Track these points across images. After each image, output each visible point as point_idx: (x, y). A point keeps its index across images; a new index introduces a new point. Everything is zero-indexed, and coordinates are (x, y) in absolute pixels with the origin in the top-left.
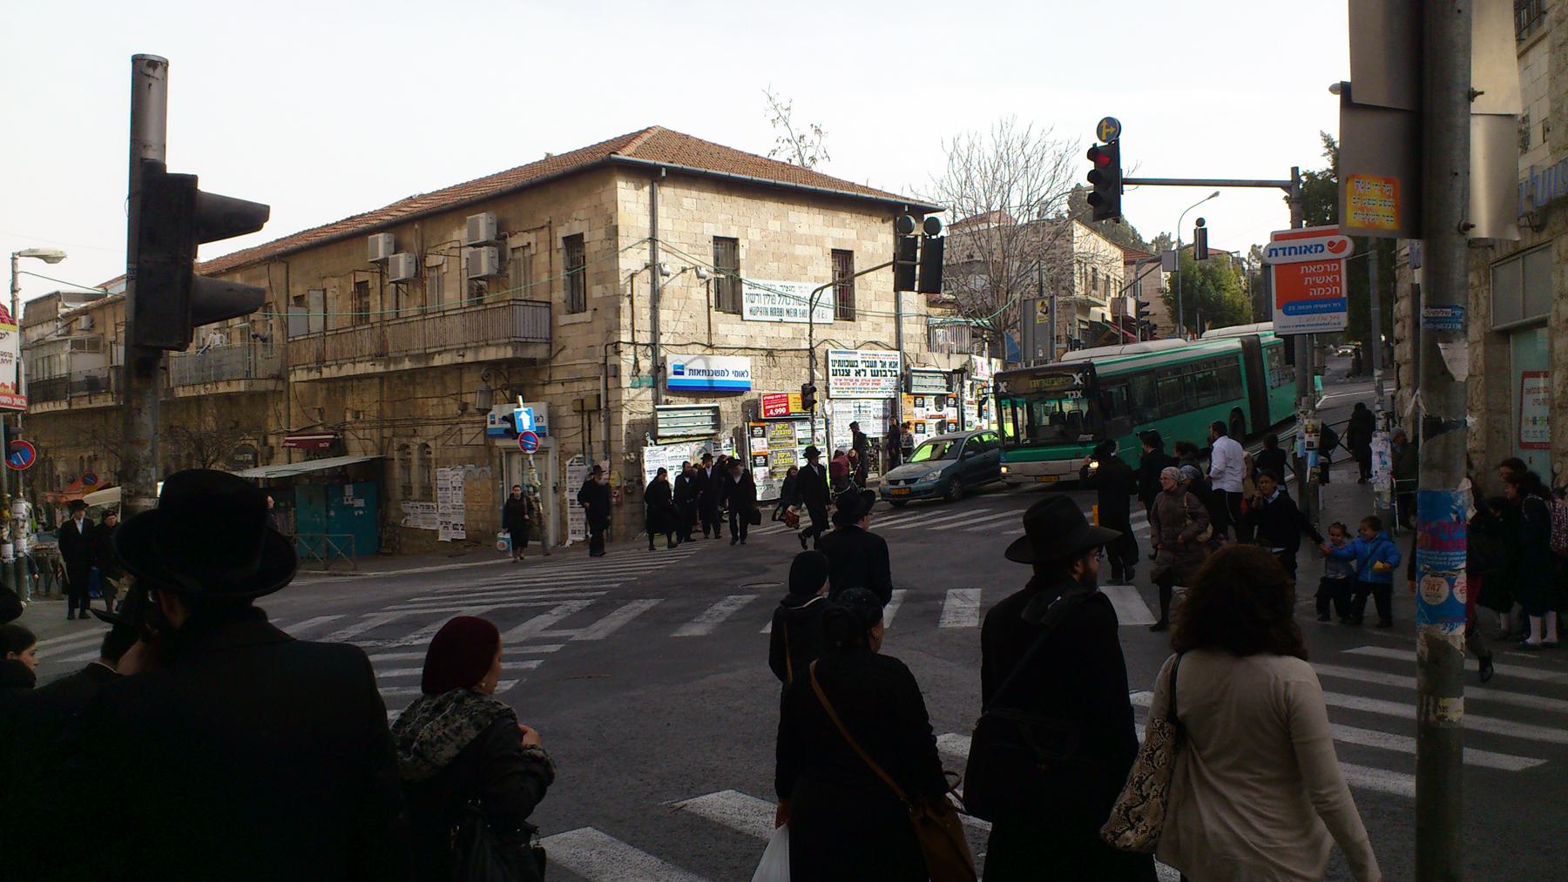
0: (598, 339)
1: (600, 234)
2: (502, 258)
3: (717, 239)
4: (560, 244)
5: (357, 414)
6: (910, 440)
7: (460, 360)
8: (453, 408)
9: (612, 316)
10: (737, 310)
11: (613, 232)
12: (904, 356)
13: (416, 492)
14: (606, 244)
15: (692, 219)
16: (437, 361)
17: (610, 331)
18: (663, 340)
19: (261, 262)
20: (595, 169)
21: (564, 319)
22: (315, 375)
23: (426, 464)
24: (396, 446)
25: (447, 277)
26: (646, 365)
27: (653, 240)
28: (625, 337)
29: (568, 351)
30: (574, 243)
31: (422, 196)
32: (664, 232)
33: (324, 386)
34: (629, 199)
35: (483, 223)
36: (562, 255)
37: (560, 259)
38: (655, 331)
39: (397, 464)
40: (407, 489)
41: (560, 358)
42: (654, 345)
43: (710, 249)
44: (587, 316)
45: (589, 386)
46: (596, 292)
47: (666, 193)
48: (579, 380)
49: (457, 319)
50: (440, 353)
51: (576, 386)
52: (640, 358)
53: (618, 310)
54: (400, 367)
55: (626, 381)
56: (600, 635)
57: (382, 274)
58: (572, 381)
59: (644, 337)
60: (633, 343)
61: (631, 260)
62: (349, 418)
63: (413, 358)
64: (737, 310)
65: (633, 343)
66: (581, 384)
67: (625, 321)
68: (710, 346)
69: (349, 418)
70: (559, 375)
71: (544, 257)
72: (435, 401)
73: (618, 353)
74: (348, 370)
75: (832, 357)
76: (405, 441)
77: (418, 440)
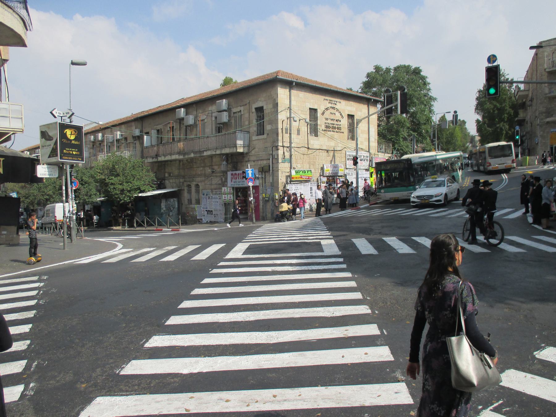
0: (269, 144)
1: (271, 106)
2: (230, 116)
3: (310, 109)
4: (254, 110)
5: (169, 174)
6: (33, 215)
7: (214, 153)
8: (209, 171)
9: (275, 136)
10: (316, 135)
11: (276, 105)
12: (370, 154)
13: (194, 201)
14: (273, 110)
15: (303, 101)
16: (205, 154)
17: (274, 142)
18: (293, 145)
19: (120, 124)
20: (271, 83)
21: (254, 138)
22: (155, 160)
23: (198, 191)
24: (185, 185)
25: (206, 124)
26: (287, 155)
27: (290, 108)
28: (280, 144)
29: (257, 150)
30: (260, 110)
31: (110, 122)
32: (291, 106)
33: (157, 164)
34: (282, 93)
35: (224, 103)
36: (255, 114)
37: (254, 116)
38: (291, 143)
39: (186, 191)
40: (190, 201)
41: (253, 152)
42: (290, 147)
43: (308, 112)
44: (265, 136)
45: (265, 162)
46: (268, 127)
47: (294, 92)
48: (261, 160)
49: (213, 138)
50: (206, 151)
51: (259, 163)
52: (285, 152)
53: (277, 134)
54: (190, 156)
55: (280, 161)
56: (204, 258)
57: (180, 123)
58: (258, 160)
59: (287, 144)
60: (283, 146)
61: (282, 116)
62: (167, 175)
63: (195, 153)
64: (316, 135)
65: (283, 146)
66: (262, 162)
67: (280, 138)
68: (308, 148)
69: (167, 175)
70: (252, 158)
71: (247, 115)
72: (201, 168)
73: (278, 149)
74: (168, 158)
75: (347, 153)
76: (189, 183)
77: (194, 183)
